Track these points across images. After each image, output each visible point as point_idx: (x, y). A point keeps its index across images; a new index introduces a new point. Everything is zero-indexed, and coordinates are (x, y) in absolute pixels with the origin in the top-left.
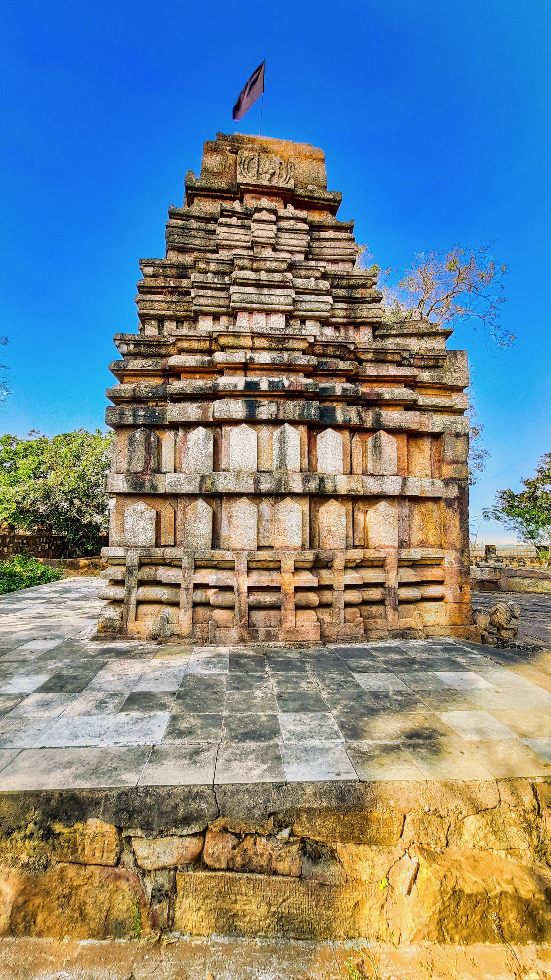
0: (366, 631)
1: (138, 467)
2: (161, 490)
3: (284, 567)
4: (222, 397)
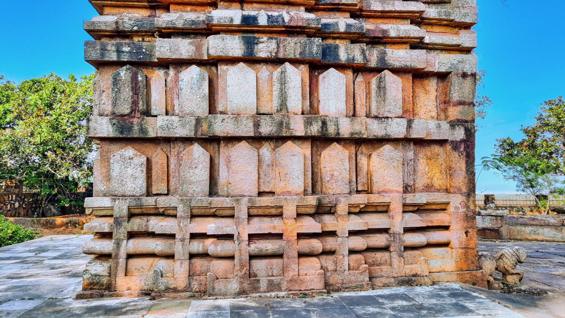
0: (371, 278)
1: (125, 109)
2: (152, 134)
3: (286, 213)
4: (217, 32)
